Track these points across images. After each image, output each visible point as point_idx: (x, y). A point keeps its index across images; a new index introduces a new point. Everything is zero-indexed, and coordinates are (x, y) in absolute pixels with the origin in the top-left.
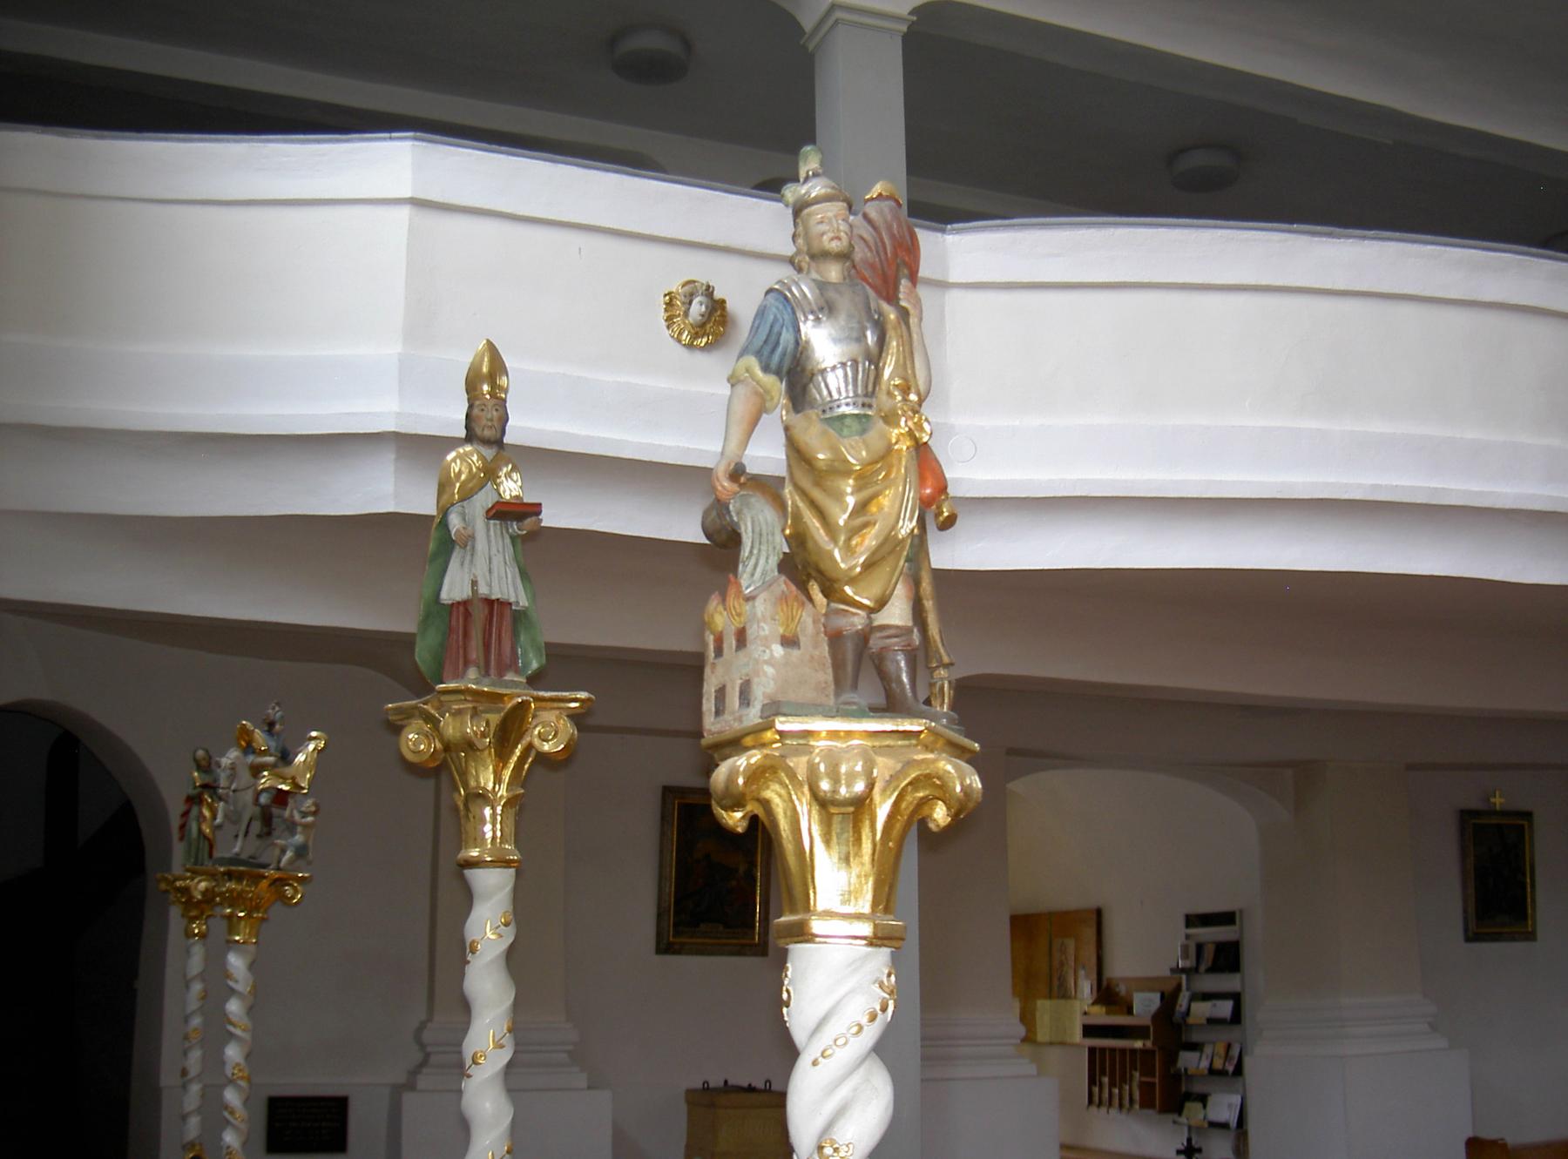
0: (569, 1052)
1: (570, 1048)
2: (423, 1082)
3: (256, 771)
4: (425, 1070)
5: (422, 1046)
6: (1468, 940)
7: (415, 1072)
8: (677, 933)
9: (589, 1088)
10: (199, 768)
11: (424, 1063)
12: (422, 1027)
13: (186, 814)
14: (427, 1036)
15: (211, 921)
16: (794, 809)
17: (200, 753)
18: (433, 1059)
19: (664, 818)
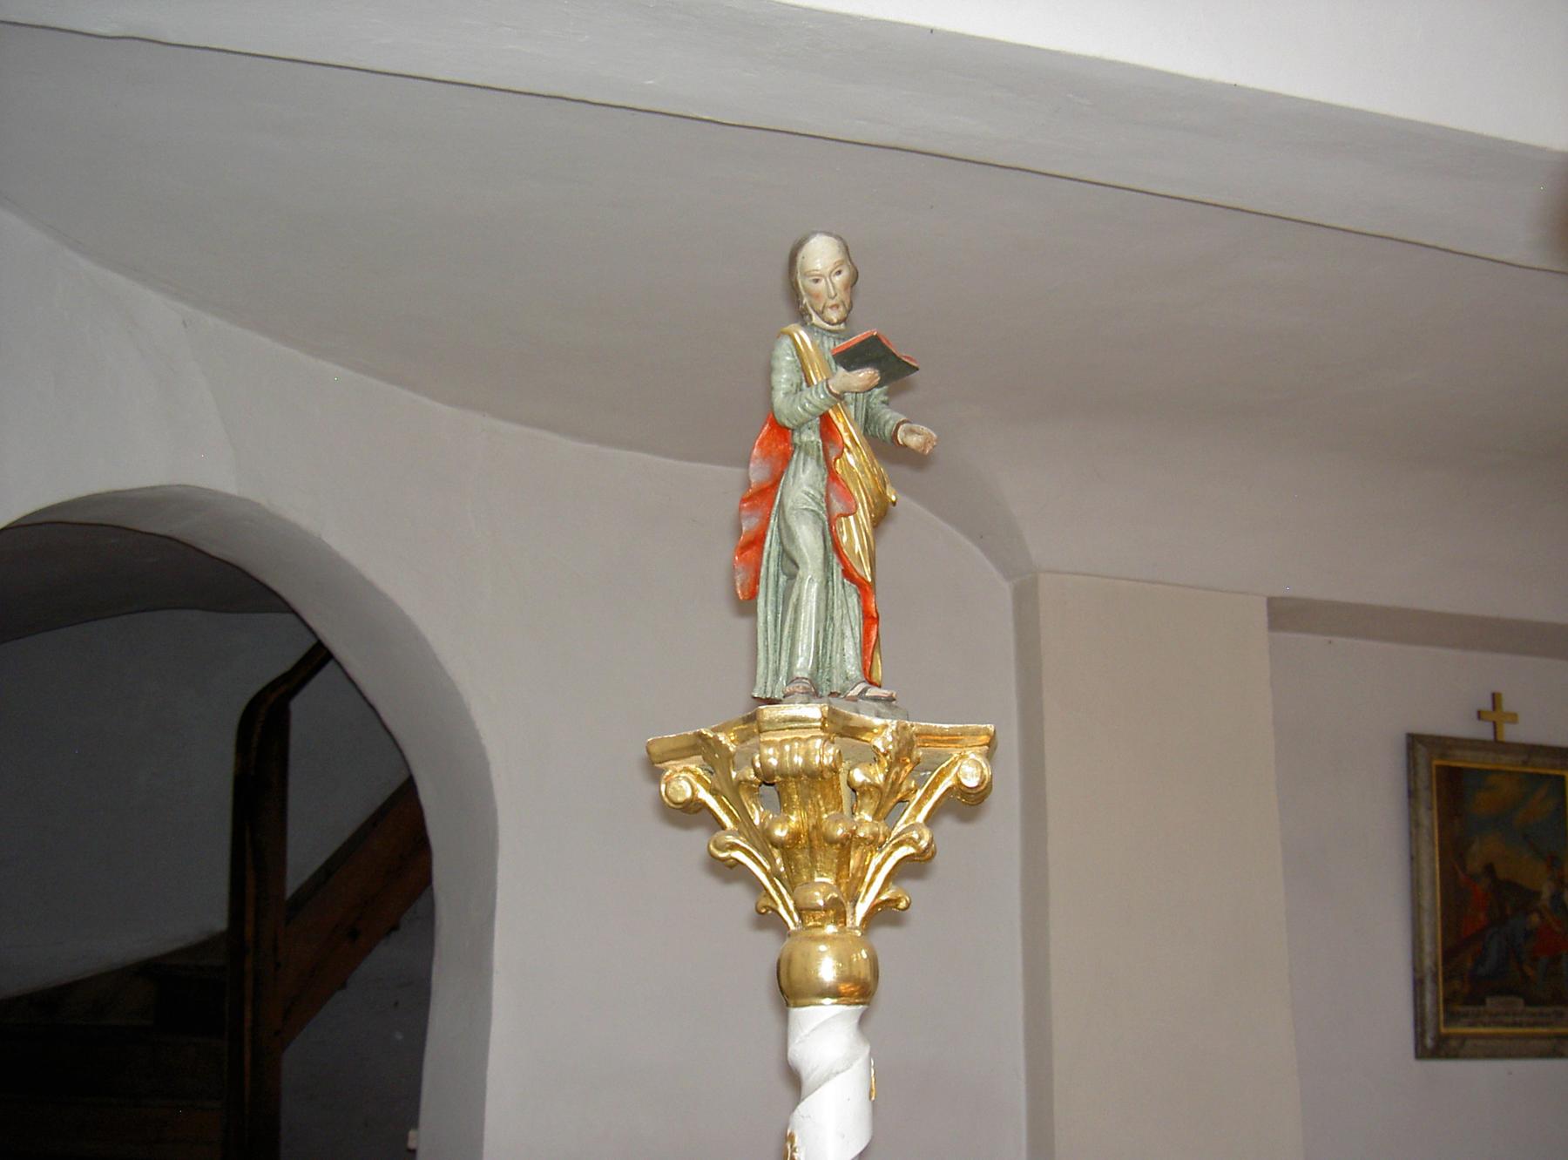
6: (1422, 1053)
8: (1451, 1017)
19: (1412, 794)
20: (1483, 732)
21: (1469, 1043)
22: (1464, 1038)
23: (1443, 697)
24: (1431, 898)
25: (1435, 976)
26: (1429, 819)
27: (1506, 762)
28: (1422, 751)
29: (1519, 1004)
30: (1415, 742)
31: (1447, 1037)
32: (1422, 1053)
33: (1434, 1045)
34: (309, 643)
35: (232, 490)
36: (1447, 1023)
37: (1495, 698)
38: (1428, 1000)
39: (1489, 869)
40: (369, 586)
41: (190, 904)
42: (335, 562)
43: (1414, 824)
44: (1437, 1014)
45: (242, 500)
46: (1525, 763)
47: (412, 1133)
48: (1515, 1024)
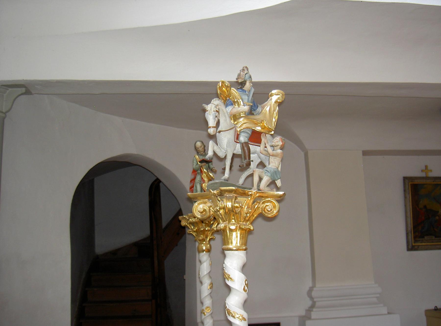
0: (377, 297)
1: (378, 295)
2: (314, 315)
3: (235, 117)
4: (314, 310)
5: (311, 298)
6: (408, 249)
7: (310, 310)
8: (416, 241)
9: (389, 313)
10: (198, 152)
11: (313, 306)
12: (311, 290)
13: (193, 180)
14: (314, 294)
15: (212, 242)
16: (242, 249)
17: (199, 144)
18: (317, 304)
19: (405, 191)
20: (423, 175)
21: (420, 247)
22: (419, 246)
23: (414, 168)
24: (410, 214)
25: (411, 232)
26: (409, 197)
27: (428, 182)
28: (407, 181)
29: (433, 237)
30: (405, 178)
31: (415, 246)
32: (408, 249)
33: (411, 248)
34: (155, 178)
35: (136, 153)
36: (414, 243)
37: (426, 167)
38: (410, 237)
39: (425, 207)
40: (165, 168)
41: (142, 231)
42: (158, 164)
43: (405, 197)
44: (412, 241)
45: (138, 155)
46: (433, 182)
47: (185, 276)
48: (432, 242)
